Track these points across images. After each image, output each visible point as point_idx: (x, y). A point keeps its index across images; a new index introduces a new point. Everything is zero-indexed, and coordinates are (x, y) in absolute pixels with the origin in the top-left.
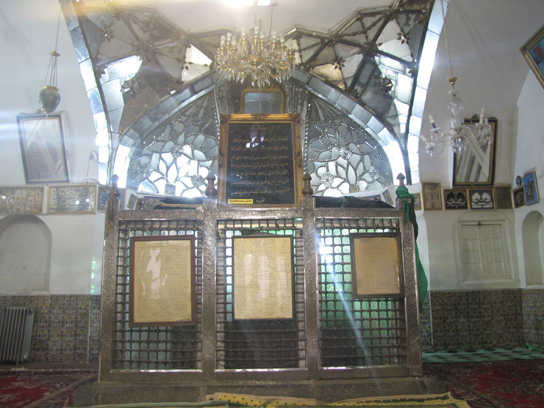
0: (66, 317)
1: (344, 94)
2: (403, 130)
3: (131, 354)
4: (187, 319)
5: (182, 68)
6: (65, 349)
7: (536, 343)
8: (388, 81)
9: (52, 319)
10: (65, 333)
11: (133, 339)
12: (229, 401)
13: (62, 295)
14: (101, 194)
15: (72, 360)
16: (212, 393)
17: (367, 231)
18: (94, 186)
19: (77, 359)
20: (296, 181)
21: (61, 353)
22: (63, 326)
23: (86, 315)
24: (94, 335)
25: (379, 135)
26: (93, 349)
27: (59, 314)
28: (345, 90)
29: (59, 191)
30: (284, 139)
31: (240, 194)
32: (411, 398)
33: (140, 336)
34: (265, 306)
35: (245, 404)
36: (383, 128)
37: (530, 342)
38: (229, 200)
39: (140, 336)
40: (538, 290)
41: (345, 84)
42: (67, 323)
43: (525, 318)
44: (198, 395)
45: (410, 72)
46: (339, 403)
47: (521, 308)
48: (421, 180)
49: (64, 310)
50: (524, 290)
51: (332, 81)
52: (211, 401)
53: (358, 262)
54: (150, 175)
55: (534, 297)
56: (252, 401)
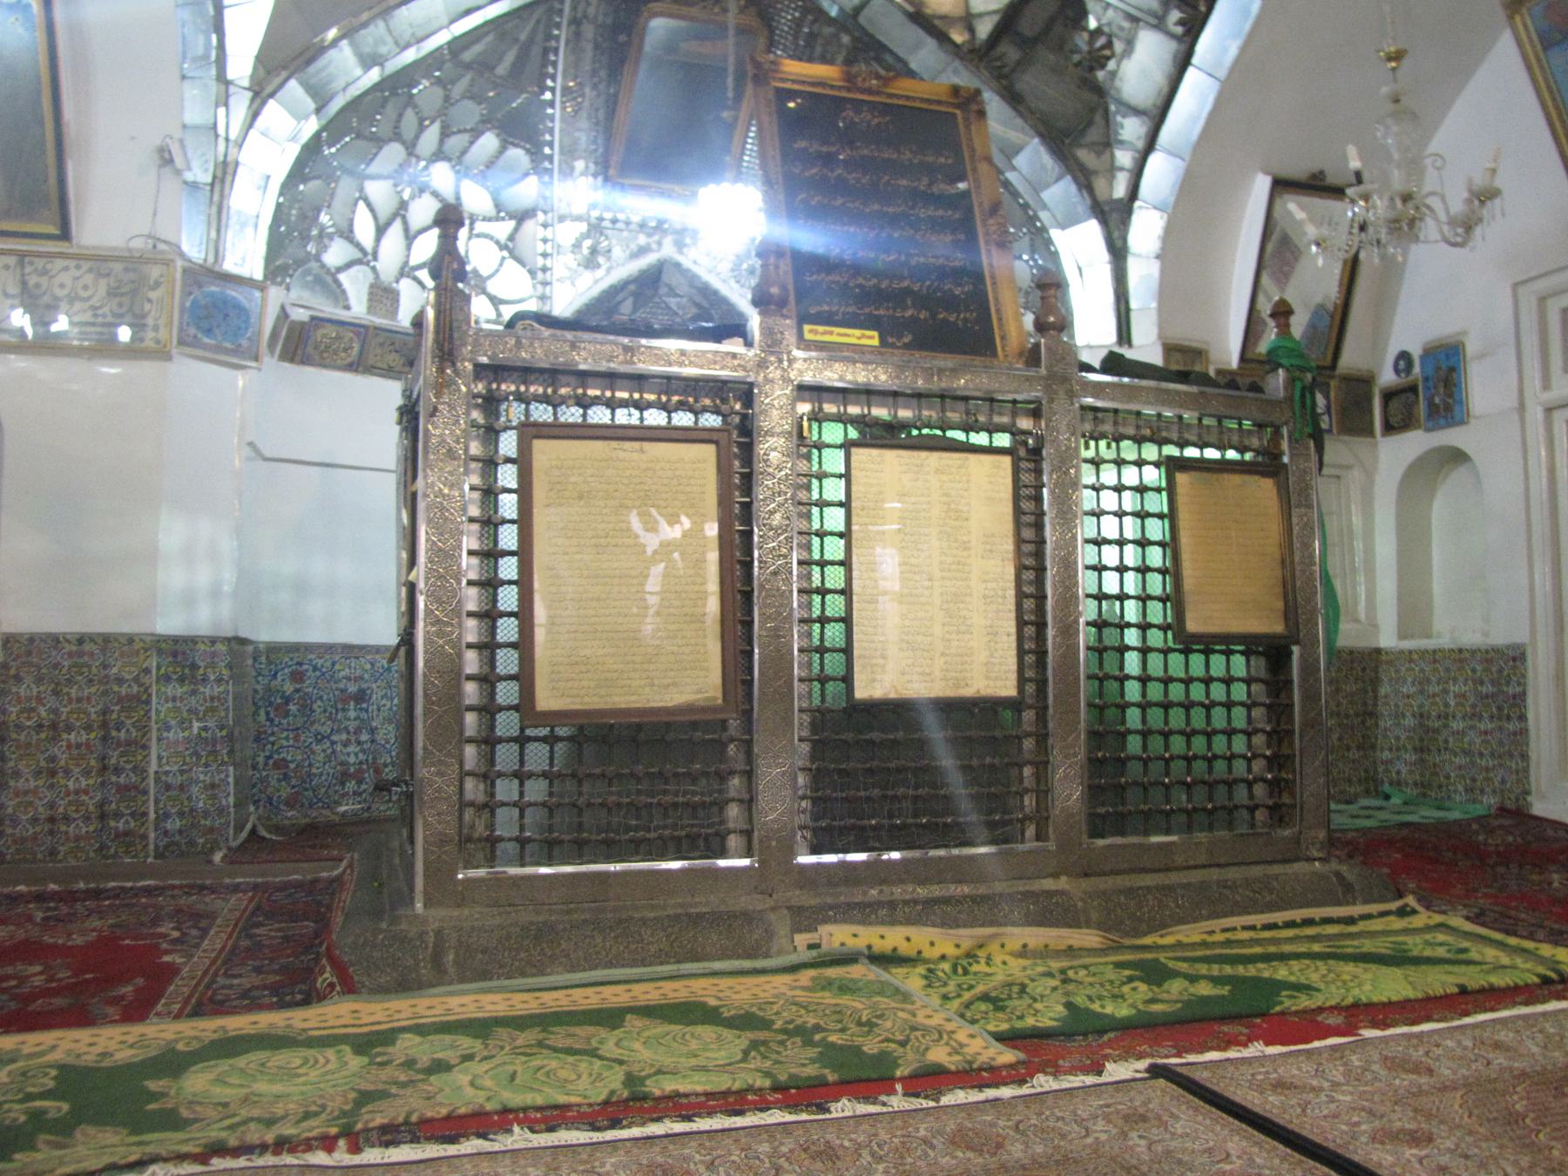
1: (962, 59)
2: (1120, 190)
3: (522, 816)
4: (707, 699)
6: (67, 819)
7: (1416, 784)
8: (1101, 42)
9: (13, 717)
10: (62, 763)
11: (498, 768)
12: (869, 947)
13: (49, 635)
14: (190, 293)
15: (92, 854)
16: (811, 929)
18: (168, 263)
19: (112, 851)
20: (995, 291)
22: (55, 739)
26: (167, 816)
27: (39, 699)
28: (972, 51)
29: (28, 269)
33: (522, 755)
34: (943, 660)
35: (913, 954)
36: (1058, 180)
37: (1398, 784)
39: (522, 755)
41: (971, 30)
42: (69, 729)
43: (1386, 722)
44: (770, 934)
45: (1181, 23)
47: (1376, 697)
48: (1160, 336)
49: (57, 684)
51: (934, 16)
52: (814, 953)
53: (1185, 540)
54: (325, 248)
55: (1422, 670)
56: (932, 944)
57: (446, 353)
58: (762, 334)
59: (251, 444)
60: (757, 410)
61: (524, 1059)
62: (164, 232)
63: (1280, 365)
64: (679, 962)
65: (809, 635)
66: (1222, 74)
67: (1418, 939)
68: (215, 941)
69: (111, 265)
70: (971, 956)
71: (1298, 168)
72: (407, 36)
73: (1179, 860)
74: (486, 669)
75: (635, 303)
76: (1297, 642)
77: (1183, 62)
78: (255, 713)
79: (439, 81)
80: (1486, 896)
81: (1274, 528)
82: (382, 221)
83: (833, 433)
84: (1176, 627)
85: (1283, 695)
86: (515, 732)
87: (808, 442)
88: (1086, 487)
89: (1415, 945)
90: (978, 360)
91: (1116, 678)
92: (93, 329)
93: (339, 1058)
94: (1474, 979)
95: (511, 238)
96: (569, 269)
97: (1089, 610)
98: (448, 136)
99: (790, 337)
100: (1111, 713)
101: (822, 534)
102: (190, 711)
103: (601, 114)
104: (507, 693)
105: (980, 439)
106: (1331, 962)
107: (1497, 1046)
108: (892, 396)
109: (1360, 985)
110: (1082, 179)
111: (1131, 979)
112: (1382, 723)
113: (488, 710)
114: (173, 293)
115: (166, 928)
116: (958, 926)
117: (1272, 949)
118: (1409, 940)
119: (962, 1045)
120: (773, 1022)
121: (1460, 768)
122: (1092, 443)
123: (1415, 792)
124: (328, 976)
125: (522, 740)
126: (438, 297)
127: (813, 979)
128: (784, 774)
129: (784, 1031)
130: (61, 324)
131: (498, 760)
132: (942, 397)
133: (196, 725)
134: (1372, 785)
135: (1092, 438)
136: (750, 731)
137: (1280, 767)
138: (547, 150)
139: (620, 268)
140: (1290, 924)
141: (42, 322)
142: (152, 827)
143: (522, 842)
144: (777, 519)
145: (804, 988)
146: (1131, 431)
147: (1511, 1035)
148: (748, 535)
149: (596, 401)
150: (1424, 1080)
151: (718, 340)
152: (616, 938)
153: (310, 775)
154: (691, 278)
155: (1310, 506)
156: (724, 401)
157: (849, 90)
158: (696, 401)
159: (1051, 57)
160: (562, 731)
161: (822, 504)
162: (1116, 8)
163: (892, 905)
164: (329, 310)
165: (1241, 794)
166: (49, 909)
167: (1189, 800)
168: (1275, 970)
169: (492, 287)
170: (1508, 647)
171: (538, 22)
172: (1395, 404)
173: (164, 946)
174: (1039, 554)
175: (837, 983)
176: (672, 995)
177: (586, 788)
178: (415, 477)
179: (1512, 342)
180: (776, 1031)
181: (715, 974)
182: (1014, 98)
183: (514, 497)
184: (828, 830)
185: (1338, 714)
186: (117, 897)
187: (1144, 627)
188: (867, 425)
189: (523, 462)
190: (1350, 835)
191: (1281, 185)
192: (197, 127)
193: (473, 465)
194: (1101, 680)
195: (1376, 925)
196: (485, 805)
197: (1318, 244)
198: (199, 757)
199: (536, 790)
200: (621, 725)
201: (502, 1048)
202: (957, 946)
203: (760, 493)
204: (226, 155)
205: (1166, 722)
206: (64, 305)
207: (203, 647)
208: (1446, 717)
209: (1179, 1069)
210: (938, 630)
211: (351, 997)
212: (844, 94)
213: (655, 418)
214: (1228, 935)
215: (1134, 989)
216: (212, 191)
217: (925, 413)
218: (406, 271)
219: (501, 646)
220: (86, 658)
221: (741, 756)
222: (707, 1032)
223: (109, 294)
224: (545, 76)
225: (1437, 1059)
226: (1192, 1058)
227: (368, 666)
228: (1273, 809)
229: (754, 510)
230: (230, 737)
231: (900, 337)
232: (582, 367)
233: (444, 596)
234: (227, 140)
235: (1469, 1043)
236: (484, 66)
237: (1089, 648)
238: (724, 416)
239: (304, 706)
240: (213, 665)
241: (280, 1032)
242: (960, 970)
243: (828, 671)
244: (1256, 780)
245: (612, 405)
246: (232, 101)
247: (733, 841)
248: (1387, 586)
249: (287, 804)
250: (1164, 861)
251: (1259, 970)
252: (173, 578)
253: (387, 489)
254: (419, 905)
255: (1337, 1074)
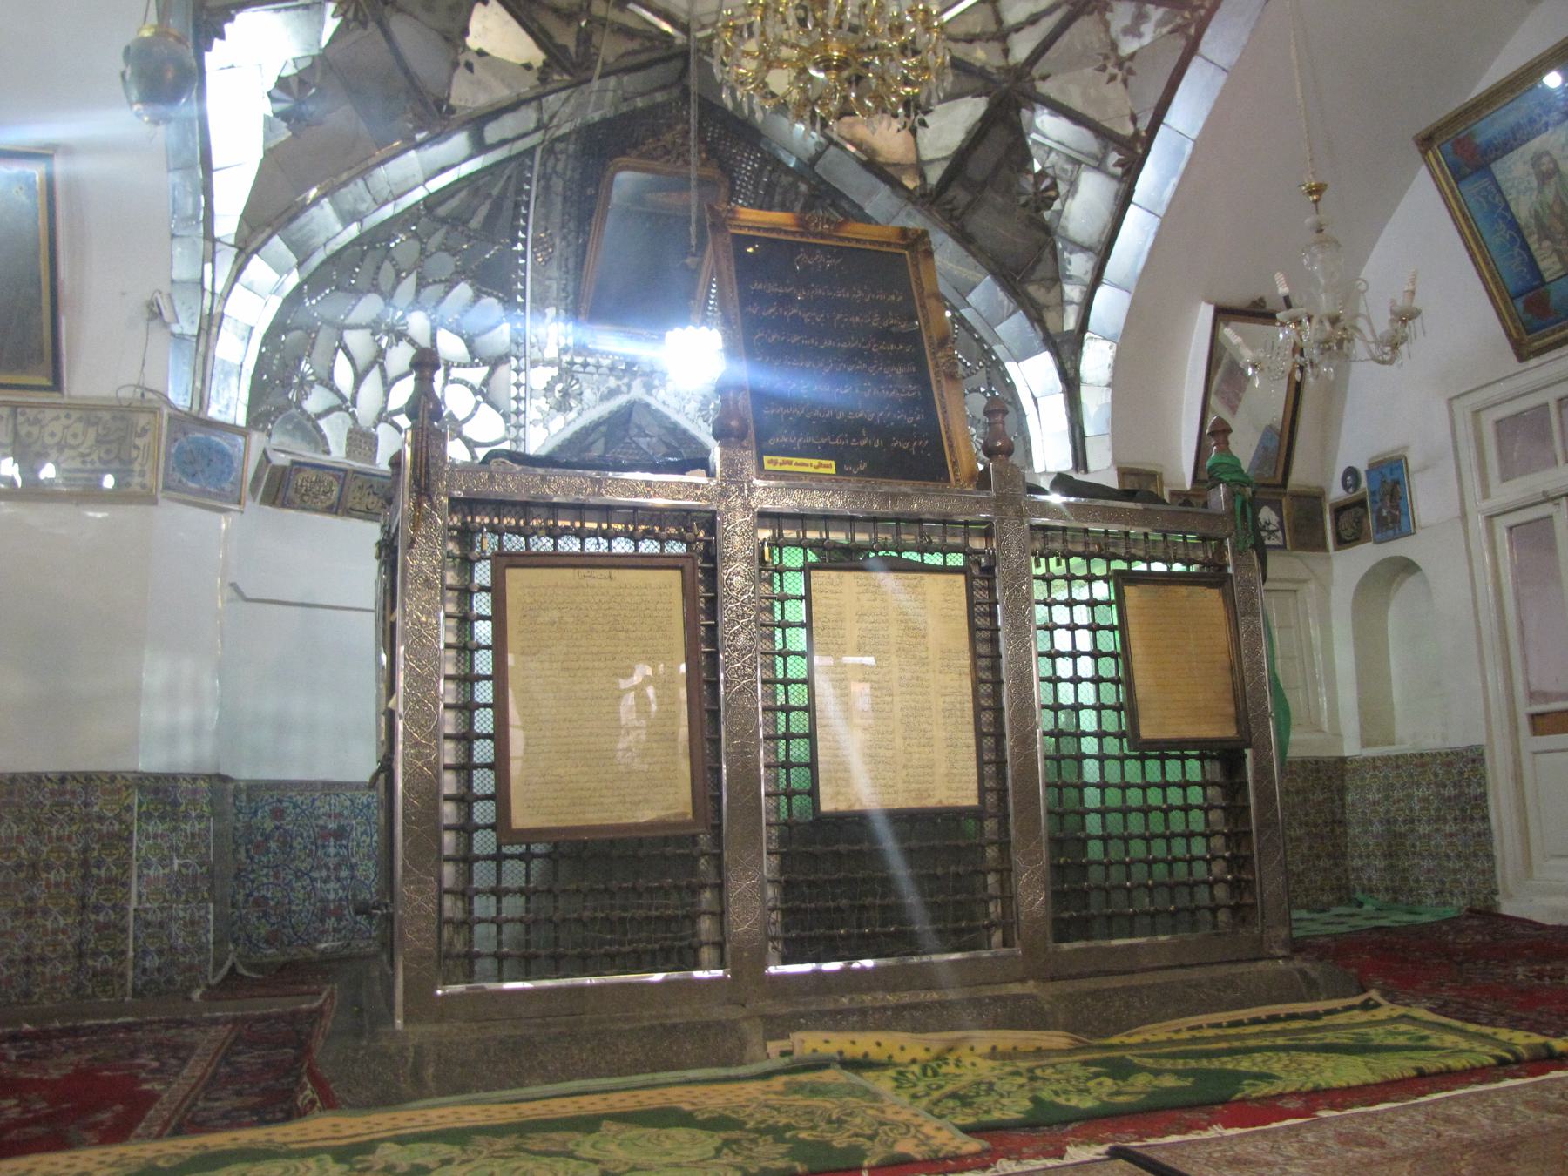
0: (45, 849)
1: (914, 203)
2: (1070, 323)
4: (676, 815)
5: (455, 65)
6: (43, 960)
7: (1387, 889)
8: (1047, 183)
10: (41, 902)
12: (841, 1053)
13: (30, 774)
14: (176, 440)
15: (68, 995)
16: (783, 1036)
17: (1149, 566)
18: (154, 411)
21: (27, 974)
22: (33, 879)
23: (121, 838)
24: (148, 905)
25: (998, 329)
26: (145, 953)
27: (19, 839)
28: (923, 196)
29: (21, 419)
30: (893, 298)
31: (795, 444)
32: (1291, 1011)
34: (905, 772)
35: (884, 1058)
36: (1014, 312)
37: (1369, 891)
38: (766, 458)
40: (1397, 757)
41: (923, 176)
42: (48, 868)
43: (1355, 830)
44: (743, 1044)
45: (1119, 164)
46: (1129, 1036)
47: (1343, 806)
48: (1114, 461)
50: (1353, 760)
52: (787, 1060)
53: (1137, 650)
55: (1386, 777)
56: (902, 1049)
57: (423, 488)
58: (723, 465)
59: (233, 585)
60: (719, 536)
61: (502, 1161)
62: (153, 382)
63: (1221, 481)
64: (654, 1071)
65: (776, 752)
66: (1161, 211)
67: (1380, 1030)
68: (195, 1069)
69: (99, 414)
70: (941, 1059)
71: (1238, 296)
72: (385, 193)
73: (1145, 962)
74: (464, 789)
75: (606, 444)
76: (1249, 746)
77: (1124, 201)
78: (235, 852)
79: (415, 235)
80: (1450, 989)
81: (1222, 638)
82: (360, 368)
83: (794, 557)
84: (1130, 734)
85: (1239, 798)
86: (492, 850)
87: (769, 566)
88: (1038, 602)
89: (1377, 1035)
90: (931, 485)
91: (1075, 786)
92: (80, 475)
93: (320, 1167)
94: (1431, 1062)
95: (485, 383)
96: (542, 412)
97: (1045, 720)
98: (424, 287)
99: (750, 468)
100: (1071, 820)
101: (785, 654)
102: (171, 848)
103: (571, 265)
104: (483, 812)
105: (935, 559)
106: (1293, 1053)
107: (1449, 1120)
108: (849, 521)
109: (1320, 1073)
110: (1033, 312)
111: (1097, 1075)
112: (1351, 831)
113: (466, 829)
114: (159, 440)
115: (146, 1059)
116: (928, 1031)
117: (1237, 1044)
118: (1371, 1031)
119: (928, 1137)
120: (745, 1123)
121: (1429, 871)
122: (1043, 561)
123: (1387, 898)
124: (309, 1093)
125: (498, 858)
126: (415, 436)
127: (785, 1084)
128: (753, 886)
129: (757, 1130)
130: (48, 472)
131: (476, 878)
132: (898, 520)
133: (177, 862)
134: (1345, 894)
135: (1041, 556)
136: (720, 846)
137: (1241, 867)
138: (519, 299)
139: (592, 409)
140: (1255, 1021)
141: (30, 469)
142: (130, 965)
143: (500, 958)
144: (742, 640)
145: (776, 1093)
146: (1080, 548)
147: (1463, 1110)
148: (713, 657)
149: (565, 531)
150: (1376, 1152)
151: (682, 472)
152: (593, 1049)
153: (290, 911)
154: (660, 418)
155: (1257, 615)
156: (689, 529)
157: (802, 234)
158: (662, 529)
159: (999, 199)
160: (538, 848)
161: (785, 625)
162: (1058, 152)
163: (863, 1012)
164: (309, 455)
165: (1202, 895)
166: (24, 1048)
167: (1152, 902)
168: (1239, 1062)
169: (468, 430)
170: (1467, 749)
171: (509, 177)
172: (1346, 518)
173: (143, 1075)
174: (995, 669)
175: (809, 1087)
176: (647, 1102)
177: (561, 903)
178: (393, 607)
179: (1451, 453)
180: (749, 1131)
181: (689, 1082)
182: (965, 239)
183: (489, 684)
184: (800, 940)
185: (1307, 824)
186: (94, 1032)
187: (1100, 735)
188: (825, 549)
189: (497, 591)
190: (1322, 940)
191: (1224, 314)
192: (183, 283)
193: (450, 594)
194: (1060, 788)
195: (1340, 1019)
196: (464, 922)
197: (1254, 367)
198: (179, 893)
199: (513, 906)
200: (593, 841)
201: (480, 1153)
202: (927, 1050)
203: (725, 617)
204: (211, 308)
205: (1125, 827)
206: (54, 453)
207: (184, 784)
208: (1412, 821)
209: (1138, 1151)
210: (899, 742)
211: (329, 1112)
212: (798, 239)
213: (622, 546)
214: (1196, 1033)
215: (1100, 1084)
216: (198, 342)
217: (881, 536)
218: (384, 416)
219: (477, 767)
220: (68, 797)
221: (712, 871)
222: (681, 1133)
223: (97, 441)
224: (516, 228)
225: (1391, 1133)
226: (1151, 1141)
227: (348, 803)
228: (1235, 909)
229: (720, 634)
230: (211, 874)
231: (855, 465)
232: (555, 500)
233: (422, 717)
234: (213, 293)
235: (1421, 1118)
236: (457, 221)
237: (1046, 757)
238: (689, 544)
239: (284, 843)
240: (194, 802)
241: (261, 1147)
242: (929, 1072)
243: (794, 785)
244: (1217, 881)
245: (581, 535)
246: (218, 258)
247: (706, 954)
248: (1348, 696)
249: (267, 941)
250: (1128, 963)
251: (1223, 1063)
252: (155, 716)
253: (366, 628)
254: (399, 1022)
255: (1292, 1150)
